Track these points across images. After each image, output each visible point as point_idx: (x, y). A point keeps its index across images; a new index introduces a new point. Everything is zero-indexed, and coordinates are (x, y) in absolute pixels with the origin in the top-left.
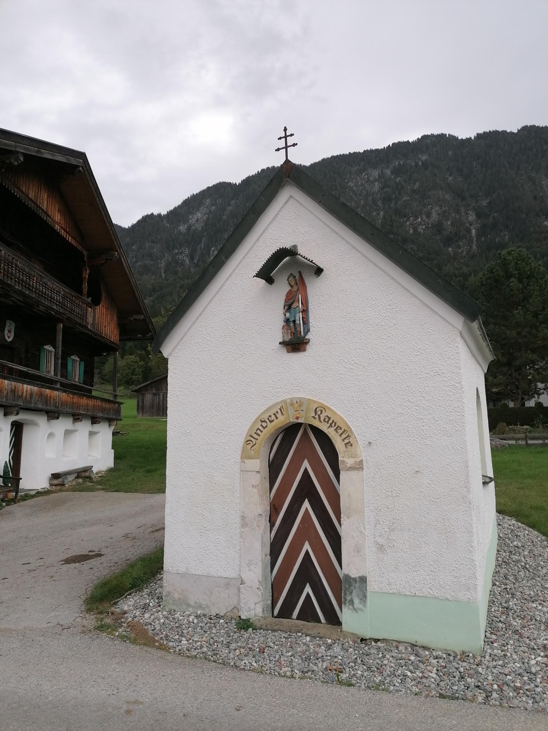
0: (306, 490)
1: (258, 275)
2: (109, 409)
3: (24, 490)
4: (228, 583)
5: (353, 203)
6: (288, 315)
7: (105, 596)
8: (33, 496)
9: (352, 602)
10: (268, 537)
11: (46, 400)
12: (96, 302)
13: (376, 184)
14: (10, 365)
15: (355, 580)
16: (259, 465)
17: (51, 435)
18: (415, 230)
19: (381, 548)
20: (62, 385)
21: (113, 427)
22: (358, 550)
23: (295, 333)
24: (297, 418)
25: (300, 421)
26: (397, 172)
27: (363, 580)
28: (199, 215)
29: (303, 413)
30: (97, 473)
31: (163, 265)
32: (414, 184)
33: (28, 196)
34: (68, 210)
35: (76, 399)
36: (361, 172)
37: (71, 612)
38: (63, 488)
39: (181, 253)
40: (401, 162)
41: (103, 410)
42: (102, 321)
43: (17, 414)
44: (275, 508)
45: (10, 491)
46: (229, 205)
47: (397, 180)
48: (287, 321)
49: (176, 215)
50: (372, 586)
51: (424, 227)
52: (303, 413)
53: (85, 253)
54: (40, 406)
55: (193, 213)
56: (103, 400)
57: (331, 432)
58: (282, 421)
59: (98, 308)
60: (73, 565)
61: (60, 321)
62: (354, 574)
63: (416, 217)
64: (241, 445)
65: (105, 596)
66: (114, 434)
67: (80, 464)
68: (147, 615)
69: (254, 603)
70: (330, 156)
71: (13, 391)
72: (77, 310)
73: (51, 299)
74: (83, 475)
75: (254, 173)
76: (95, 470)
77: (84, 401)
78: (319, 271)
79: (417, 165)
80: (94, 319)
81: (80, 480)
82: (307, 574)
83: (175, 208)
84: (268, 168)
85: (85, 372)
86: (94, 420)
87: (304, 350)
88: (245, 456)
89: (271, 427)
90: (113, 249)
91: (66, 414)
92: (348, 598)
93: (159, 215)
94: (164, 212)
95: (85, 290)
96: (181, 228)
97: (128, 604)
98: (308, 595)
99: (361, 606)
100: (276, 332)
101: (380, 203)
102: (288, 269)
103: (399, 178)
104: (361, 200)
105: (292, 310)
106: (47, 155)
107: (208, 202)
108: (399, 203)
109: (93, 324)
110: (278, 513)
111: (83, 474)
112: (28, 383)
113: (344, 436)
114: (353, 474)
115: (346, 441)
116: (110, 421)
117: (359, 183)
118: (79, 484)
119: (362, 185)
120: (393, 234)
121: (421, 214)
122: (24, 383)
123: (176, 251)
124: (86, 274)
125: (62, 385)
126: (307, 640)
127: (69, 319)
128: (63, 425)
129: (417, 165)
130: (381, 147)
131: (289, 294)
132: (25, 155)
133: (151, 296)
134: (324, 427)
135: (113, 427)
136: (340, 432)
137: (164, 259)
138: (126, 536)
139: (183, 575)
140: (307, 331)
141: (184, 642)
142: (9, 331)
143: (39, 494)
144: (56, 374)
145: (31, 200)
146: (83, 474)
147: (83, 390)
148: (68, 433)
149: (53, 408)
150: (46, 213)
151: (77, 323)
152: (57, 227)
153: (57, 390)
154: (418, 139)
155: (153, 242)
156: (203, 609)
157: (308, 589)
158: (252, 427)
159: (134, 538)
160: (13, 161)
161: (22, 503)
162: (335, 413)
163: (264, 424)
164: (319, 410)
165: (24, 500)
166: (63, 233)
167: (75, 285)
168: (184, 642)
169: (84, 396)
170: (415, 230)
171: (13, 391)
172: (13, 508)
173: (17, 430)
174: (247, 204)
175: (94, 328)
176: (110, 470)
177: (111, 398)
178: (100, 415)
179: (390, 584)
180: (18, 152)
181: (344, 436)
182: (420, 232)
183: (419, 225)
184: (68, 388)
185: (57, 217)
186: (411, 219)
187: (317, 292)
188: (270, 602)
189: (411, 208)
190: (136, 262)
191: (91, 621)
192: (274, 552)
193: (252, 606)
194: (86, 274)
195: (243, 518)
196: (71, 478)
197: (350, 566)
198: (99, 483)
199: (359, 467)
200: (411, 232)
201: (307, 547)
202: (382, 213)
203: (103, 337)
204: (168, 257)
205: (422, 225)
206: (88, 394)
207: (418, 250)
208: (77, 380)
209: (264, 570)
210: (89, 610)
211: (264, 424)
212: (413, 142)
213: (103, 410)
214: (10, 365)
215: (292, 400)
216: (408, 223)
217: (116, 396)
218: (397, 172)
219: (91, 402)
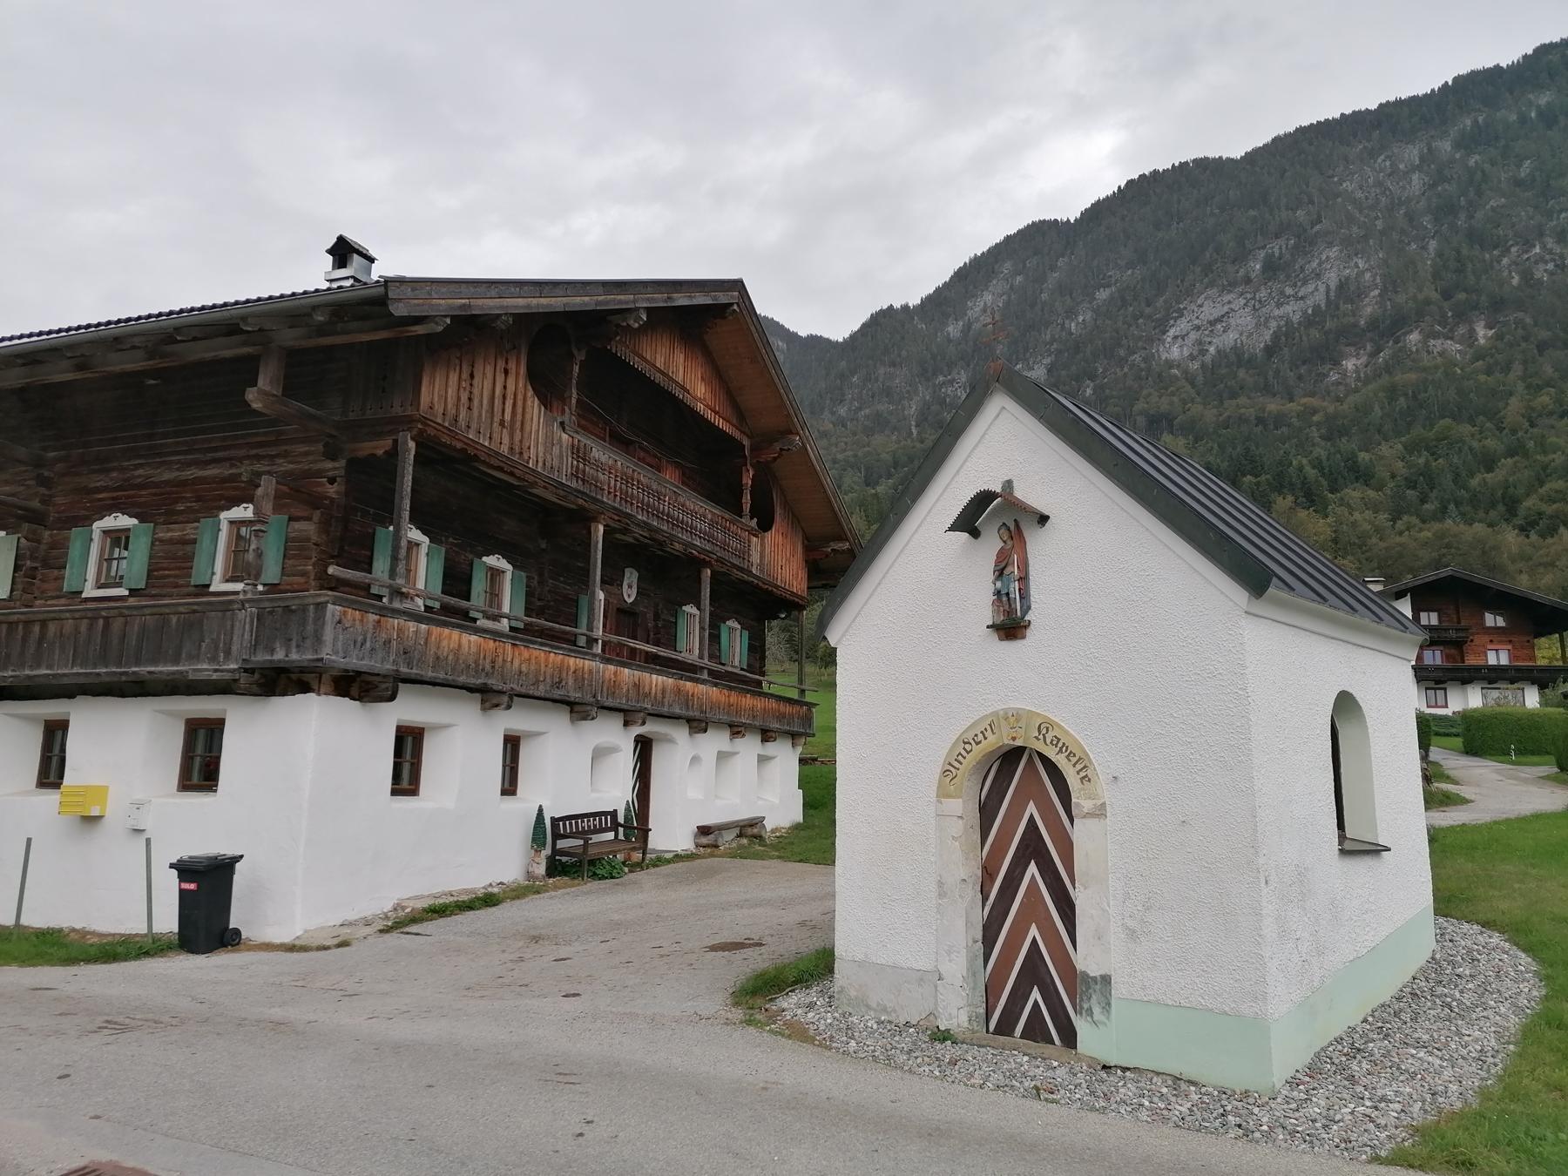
0: (1032, 848)
1: (952, 528)
2: (792, 716)
3: (654, 851)
4: (921, 977)
5: (1355, 229)
6: (999, 584)
7: (761, 992)
8: (669, 861)
9: (1090, 1012)
10: (979, 916)
11: (687, 700)
12: (765, 525)
13: (1415, 177)
14: (632, 643)
15: (1094, 979)
16: (962, 807)
17: (695, 760)
18: (1527, 276)
19: (1132, 934)
20: (711, 673)
21: (799, 749)
22: (1099, 936)
23: (1010, 612)
24: (1014, 739)
25: (1019, 743)
26: (1467, 143)
27: (1106, 980)
28: (988, 297)
29: (1022, 732)
30: (773, 831)
31: (913, 409)
32: (1519, 166)
33: (654, 366)
34: (719, 376)
35: (734, 698)
36: (1373, 154)
37: (715, 1003)
38: (716, 851)
39: (951, 382)
40: (1480, 119)
41: (781, 717)
42: (776, 558)
43: (644, 723)
44: (988, 873)
45: (634, 849)
46: (1053, 268)
47: (1472, 162)
48: (998, 593)
49: (941, 302)
50: (1119, 990)
51: (1550, 266)
52: (1022, 732)
53: (746, 442)
54: (677, 710)
55: (975, 296)
56: (780, 698)
57: (1060, 761)
58: (992, 742)
59: (768, 534)
60: (720, 954)
61: (706, 564)
62: (1094, 971)
63: (1529, 245)
64: (937, 777)
65: (761, 992)
66: (802, 761)
67: (744, 814)
68: (811, 1015)
69: (957, 1007)
70: (1291, 129)
71: (637, 686)
72: (734, 544)
73: (691, 530)
74: (749, 830)
75: (1110, 193)
76: (769, 825)
77: (748, 701)
78: (1043, 519)
79: (1523, 120)
80: (762, 557)
81: (745, 841)
82: (1034, 971)
83: (938, 290)
84: (1142, 176)
85: (751, 648)
86: (766, 736)
87: (1024, 637)
88: (943, 793)
89: (978, 752)
90: (790, 432)
91: (719, 724)
92: (1086, 1006)
93: (905, 308)
94: (914, 301)
95: (747, 507)
96: (950, 329)
97: (791, 1003)
98: (1036, 1002)
99: (1103, 1018)
100: (984, 612)
101: (1426, 221)
102: (997, 517)
103: (1477, 157)
104: (1377, 218)
105: (1005, 578)
106: (681, 300)
107: (1007, 267)
108: (1479, 215)
109: (761, 564)
110: (993, 881)
111: (749, 831)
112: (659, 673)
113: (1079, 767)
114: (1091, 823)
115: (1082, 774)
116: (794, 736)
117: (1371, 181)
118: (741, 847)
119: (1379, 184)
120: (1465, 290)
121: (1541, 235)
122: (652, 671)
123: (941, 378)
124: (747, 480)
125: (711, 673)
126: (1020, 1058)
127: (720, 560)
128: (714, 742)
129: (1523, 120)
130: (1422, 89)
131: (1001, 552)
132: (649, 310)
133: (889, 476)
134: (1051, 753)
135: (799, 749)
136: (1074, 760)
137: (916, 399)
138: (803, 924)
139: (860, 964)
140: (1027, 608)
141: (853, 1043)
142: (630, 587)
143: (678, 858)
144: (701, 657)
145: (660, 371)
146: (749, 831)
147: (748, 681)
148: (722, 756)
149: (697, 714)
150: (683, 388)
151: (734, 566)
152: (700, 407)
153: (703, 682)
154: (1525, 57)
155: (893, 364)
156: (888, 1013)
157: (1036, 995)
158: (951, 750)
159: (814, 927)
160: (631, 322)
161: (652, 870)
162: (1067, 732)
163: (968, 747)
164: (1045, 727)
165: (655, 866)
166: (709, 415)
167: (727, 497)
168: (853, 1043)
169: (748, 691)
170: (1527, 276)
171: (637, 686)
172: (639, 875)
173: (644, 748)
174: (1095, 262)
175: (762, 571)
176: (796, 827)
177: (794, 695)
178: (775, 725)
179: (1144, 988)
180: (637, 309)
181: (1079, 767)
182: (1540, 282)
183: (1536, 263)
184: (718, 678)
185: (700, 390)
186: (1514, 249)
187: (1039, 546)
188: (982, 1011)
189: (1513, 225)
190: (860, 409)
191: (738, 1014)
192: (989, 939)
193: (954, 1012)
194: (747, 480)
195: (940, 884)
196: (729, 836)
197: (1086, 959)
198: (773, 846)
199: (1100, 812)
200: (1516, 281)
201: (1034, 932)
202: (1433, 245)
203: (777, 587)
204: (924, 393)
205: (1546, 262)
206: (755, 688)
207: (1536, 324)
208: (737, 663)
209: (971, 961)
210: (736, 1004)
211: (968, 747)
212: (1511, 67)
213: (781, 717)
214: (632, 643)
215: (1006, 711)
216: (1505, 261)
217: (803, 691)
218: (1467, 143)
219: (759, 703)
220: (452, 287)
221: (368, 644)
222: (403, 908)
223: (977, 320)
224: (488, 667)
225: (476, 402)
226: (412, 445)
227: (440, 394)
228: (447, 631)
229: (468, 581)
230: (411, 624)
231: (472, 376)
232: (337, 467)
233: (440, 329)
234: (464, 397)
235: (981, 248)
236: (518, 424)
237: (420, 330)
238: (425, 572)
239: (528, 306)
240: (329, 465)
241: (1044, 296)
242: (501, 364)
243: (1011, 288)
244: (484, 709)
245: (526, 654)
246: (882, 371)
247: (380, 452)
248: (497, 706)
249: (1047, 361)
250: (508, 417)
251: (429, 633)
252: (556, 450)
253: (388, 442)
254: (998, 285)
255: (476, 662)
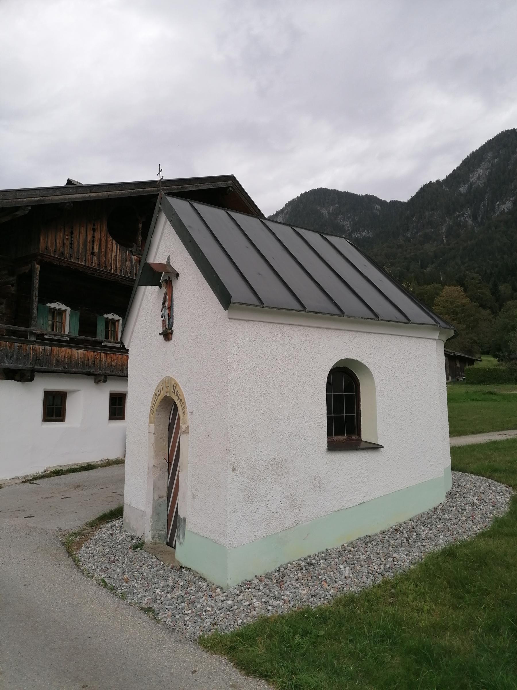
39: (463, 215)
49: (455, 177)
55: (473, 171)
93: (438, 182)
96: (461, 189)
107: (490, 155)
133: (433, 263)
190: (417, 233)
204: (449, 221)
220: (37, 192)
221: (15, 357)
222: (48, 471)
223: (475, 183)
224: (90, 364)
225: (75, 245)
226: (38, 267)
227: (52, 243)
228: (63, 349)
229: (95, 326)
230: (41, 347)
231: (72, 233)
232: (12, 279)
233: (27, 212)
234: (68, 243)
235: (475, 147)
236: (103, 254)
237: (19, 213)
238: (69, 325)
239: (84, 197)
240: (11, 279)
241: (510, 167)
242: (90, 227)
243: (492, 164)
244: (95, 382)
245: (114, 357)
246: (427, 213)
247: (27, 271)
248: (100, 381)
249: (513, 199)
250: (96, 250)
251: (52, 351)
252: (128, 264)
253: (29, 266)
254: (485, 165)
255: (83, 362)
